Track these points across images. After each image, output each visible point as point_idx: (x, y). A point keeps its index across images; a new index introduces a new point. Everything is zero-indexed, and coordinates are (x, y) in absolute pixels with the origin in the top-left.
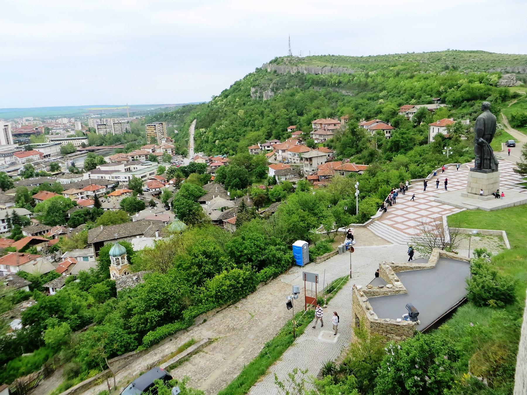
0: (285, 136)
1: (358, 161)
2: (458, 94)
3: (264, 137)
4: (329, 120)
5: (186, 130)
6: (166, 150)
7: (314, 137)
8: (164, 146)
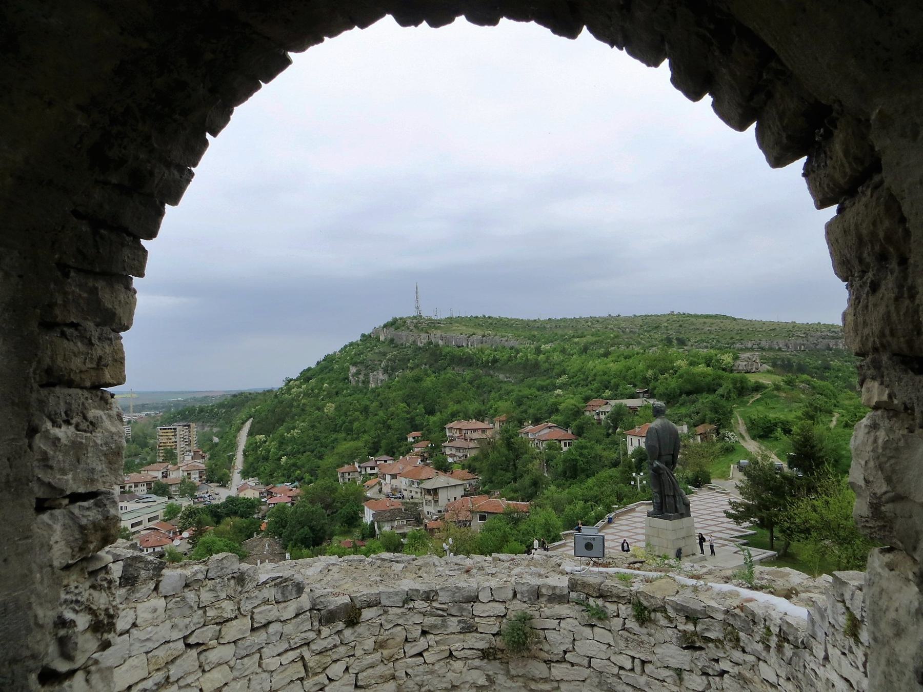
0: (402, 449)
1: (512, 495)
2: (673, 383)
3: (366, 451)
4: (474, 424)
5: (231, 437)
6: (189, 474)
7: (448, 452)
8: (189, 466)
